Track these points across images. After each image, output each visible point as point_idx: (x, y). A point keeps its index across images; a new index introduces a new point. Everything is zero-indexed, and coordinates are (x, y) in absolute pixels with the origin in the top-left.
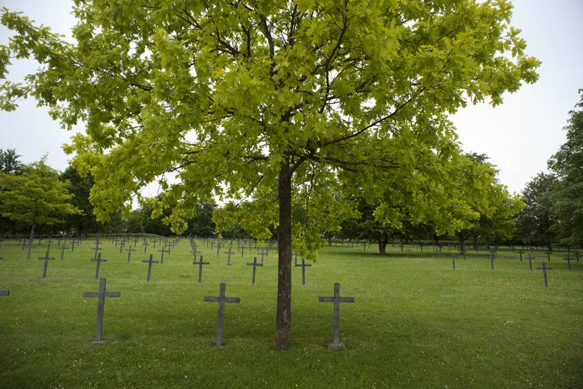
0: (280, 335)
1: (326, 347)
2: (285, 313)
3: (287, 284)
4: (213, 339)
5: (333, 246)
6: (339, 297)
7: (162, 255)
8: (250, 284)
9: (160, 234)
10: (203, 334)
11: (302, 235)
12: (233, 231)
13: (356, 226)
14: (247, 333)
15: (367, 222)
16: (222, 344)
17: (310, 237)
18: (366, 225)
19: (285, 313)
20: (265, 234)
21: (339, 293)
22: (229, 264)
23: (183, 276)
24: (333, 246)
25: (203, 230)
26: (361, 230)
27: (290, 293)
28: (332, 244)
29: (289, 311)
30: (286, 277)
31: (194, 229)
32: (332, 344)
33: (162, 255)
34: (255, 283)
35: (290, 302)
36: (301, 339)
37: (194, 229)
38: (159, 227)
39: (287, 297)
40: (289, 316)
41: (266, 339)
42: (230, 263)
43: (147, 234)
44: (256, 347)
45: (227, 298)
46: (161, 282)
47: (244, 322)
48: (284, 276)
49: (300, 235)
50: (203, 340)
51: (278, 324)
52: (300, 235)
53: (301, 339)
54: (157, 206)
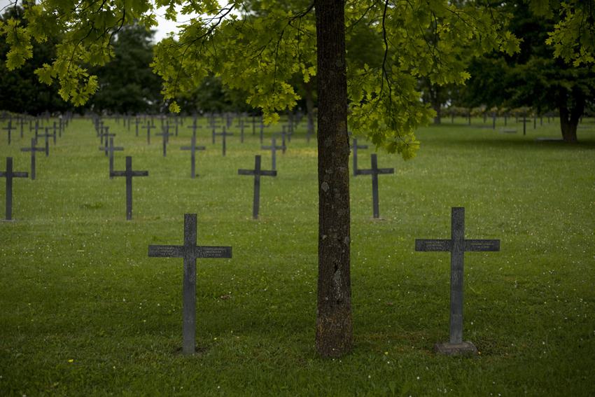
0: (326, 326)
1: (434, 350)
2: (337, 277)
3: (340, 213)
4: (175, 339)
8: (249, 218)
9: (18, 110)
10: (152, 330)
11: (374, 95)
13: (503, 72)
14: (251, 325)
16: (197, 350)
17: (395, 99)
19: (337, 277)
23: (88, 206)
26: (517, 82)
29: (347, 272)
30: (338, 195)
32: (446, 345)
34: (261, 218)
36: (375, 335)
39: (340, 241)
40: (347, 283)
41: (294, 337)
48: (333, 194)
49: (369, 96)
51: (321, 303)
52: (369, 96)
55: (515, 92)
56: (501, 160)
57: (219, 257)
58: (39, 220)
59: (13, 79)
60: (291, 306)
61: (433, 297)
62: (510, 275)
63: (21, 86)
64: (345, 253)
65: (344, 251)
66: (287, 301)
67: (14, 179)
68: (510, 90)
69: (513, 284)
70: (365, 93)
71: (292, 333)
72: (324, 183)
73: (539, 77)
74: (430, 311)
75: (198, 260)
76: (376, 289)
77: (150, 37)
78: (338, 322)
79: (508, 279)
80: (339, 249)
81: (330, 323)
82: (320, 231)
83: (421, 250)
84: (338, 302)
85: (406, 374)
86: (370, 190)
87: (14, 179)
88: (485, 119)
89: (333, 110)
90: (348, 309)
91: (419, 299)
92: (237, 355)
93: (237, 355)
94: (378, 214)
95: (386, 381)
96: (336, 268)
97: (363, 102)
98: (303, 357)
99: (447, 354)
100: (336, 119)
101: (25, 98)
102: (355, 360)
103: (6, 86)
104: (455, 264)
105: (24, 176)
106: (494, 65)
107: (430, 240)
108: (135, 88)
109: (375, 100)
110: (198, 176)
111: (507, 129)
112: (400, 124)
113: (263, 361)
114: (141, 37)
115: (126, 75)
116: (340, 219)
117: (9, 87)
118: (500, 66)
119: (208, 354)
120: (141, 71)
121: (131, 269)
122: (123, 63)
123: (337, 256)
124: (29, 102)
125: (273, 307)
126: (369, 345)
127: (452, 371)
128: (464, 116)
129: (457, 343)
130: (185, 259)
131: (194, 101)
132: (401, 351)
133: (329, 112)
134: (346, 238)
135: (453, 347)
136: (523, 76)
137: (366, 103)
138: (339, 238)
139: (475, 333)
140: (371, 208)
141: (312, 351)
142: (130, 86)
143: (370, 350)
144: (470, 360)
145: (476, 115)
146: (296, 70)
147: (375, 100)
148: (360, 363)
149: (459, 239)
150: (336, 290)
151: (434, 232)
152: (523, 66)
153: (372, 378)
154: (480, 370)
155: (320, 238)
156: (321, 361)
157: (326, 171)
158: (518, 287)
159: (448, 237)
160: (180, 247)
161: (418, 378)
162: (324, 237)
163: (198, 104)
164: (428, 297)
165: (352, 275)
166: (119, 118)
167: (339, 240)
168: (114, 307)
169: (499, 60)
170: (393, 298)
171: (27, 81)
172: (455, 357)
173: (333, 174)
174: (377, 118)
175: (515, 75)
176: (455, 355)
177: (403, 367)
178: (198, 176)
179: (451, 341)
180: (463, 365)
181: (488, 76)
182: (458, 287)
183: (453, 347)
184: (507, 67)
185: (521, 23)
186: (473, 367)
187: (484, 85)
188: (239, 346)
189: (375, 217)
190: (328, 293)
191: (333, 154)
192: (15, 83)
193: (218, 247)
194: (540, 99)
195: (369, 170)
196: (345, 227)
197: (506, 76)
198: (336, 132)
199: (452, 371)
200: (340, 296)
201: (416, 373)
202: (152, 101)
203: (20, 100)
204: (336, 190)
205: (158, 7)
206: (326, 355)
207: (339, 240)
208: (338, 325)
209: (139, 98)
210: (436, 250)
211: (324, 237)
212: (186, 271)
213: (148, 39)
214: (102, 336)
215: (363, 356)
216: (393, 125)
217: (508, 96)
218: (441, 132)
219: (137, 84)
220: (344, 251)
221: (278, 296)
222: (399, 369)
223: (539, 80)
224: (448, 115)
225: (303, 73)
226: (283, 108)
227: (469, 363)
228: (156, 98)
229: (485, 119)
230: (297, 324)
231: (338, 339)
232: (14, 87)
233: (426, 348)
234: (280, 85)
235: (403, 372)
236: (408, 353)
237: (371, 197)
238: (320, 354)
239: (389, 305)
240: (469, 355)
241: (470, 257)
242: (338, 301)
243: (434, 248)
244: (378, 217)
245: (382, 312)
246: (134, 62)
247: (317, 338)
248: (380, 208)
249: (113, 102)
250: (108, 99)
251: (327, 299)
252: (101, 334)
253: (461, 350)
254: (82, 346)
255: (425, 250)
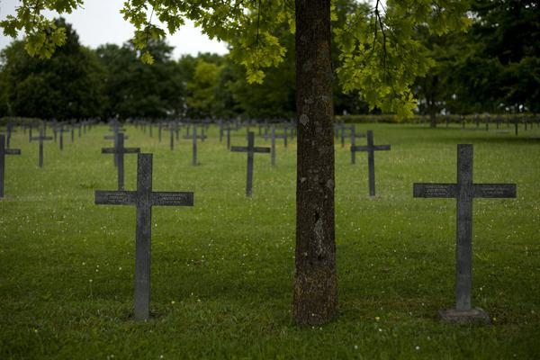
0: (305, 286)
1: (436, 318)
2: (318, 228)
3: (322, 150)
4: (129, 304)
5: (439, 128)
6: (471, 184)
7: (41, 147)
8: (241, 194)
9: (47, 117)
10: (98, 293)
11: (367, 47)
12: (209, 106)
13: (497, 71)
14: (222, 290)
15: (524, 61)
16: (152, 315)
17: (390, 50)
18: (522, 67)
19: (318, 228)
20: (267, 50)
21: (471, 172)
22: (195, 163)
23: (83, 186)
24: (439, 128)
25: (142, 107)
26: (510, 80)
27: (331, 175)
28: (438, 125)
29: (330, 223)
30: (319, 130)
31: (123, 105)
32: (451, 312)
33: (41, 147)
34: (254, 196)
35: (332, 198)
36: (366, 302)
37: (123, 105)
38: (44, 103)
39: (323, 184)
40: (330, 235)
41: (269, 303)
42: (200, 158)
43: (19, 119)
44: (241, 320)
45: (159, 194)
46: (31, 198)
47: (216, 268)
48: (313, 128)
49: (361, 47)
50: (101, 305)
51: (300, 259)
52: (361, 47)
53: (366, 302)
54: (190, 340)
55: (508, 91)
56: (497, 152)
57: (178, 205)
58: (31, 198)
59: (44, 90)
60: (270, 271)
61: (434, 263)
62: (518, 244)
63: (52, 96)
64: (328, 199)
65: (326, 197)
66: (267, 266)
67: (6, 156)
68: (505, 88)
69: (523, 252)
70: (358, 43)
71: (268, 299)
72: (304, 115)
73: (532, 74)
74: (431, 277)
75: (153, 207)
76: (369, 256)
77: (169, 52)
78: (319, 282)
79: (516, 247)
80: (321, 194)
81: (310, 284)
82: (299, 173)
83: (420, 196)
84: (320, 258)
85: (402, 344)
86: (367, 172)
87: (6, 156)
88: (478, 124)
89: (314, 27)
90: (332, 267)
91: (418, 266)
92: (197, 321)
93: (197, 321)
94: (374, 191)
95: (376, 352)
96: (317, 217)
97: (356, 53)
98: (276, 324)
99: (453, 322)
100: (317, 38)
101: (55, 108)
102: (340, 328)
103: (38, 96)
104: (462, 213)
105: (16, 153)
106: (488, 65)
107: (430, 184)
108: (155, 99)
109: (368, 52)
110: (199, 164)
111: (500, 131)
112: (395, 79)
113: (227, 328)
114: (161, 53)
115: (147, 88)
116: (322, 157)
117: (40, 98)
118: (494, 65)
119: (163, 320)
120: (162, 83)
121: (105, 236)
122: (144, 76)
123: (318, 203)
124: (58, 111)
125: (250, 272)
126: (358, 312)
127: (460, 342)
128: (458, 122)
129: (465, 310)
130: (138, 206)
131: (208, 112)
132: (396, 319)
133: (308, 30)
134: (329, 182)
135: (459, 314)
136: (517, 74)
137: (358, 54)
138: (321, 181)
139: (485, 300)
140: (367, 186)
141: (288, 317)
142: (150, 97)
143: (358, 318)
144: (482, 329)
145: (469, 121)
146: (282, 19)
147: (368, 52)
148: (346, 331)
149: (466, 182)
150: (317, 244)
151: (432, 207)
152: (516, 64)
153: (360, 349)
154: (495, 340)
155: (299, 181)
156: (298, 328)
157: (306, 101)
158: (529, 255)
159: (454, 180)
160: (132, 193)
161: (418, 348)
162: (303, 179)
163: (212, 113)
164: (427, 264)
165: (339, 241)
166: (145, 125)
167: (321, 184)
168: (72, 271)
169: (494, 59)
170: (388, 264)
171: (57, 93)
172: (462, 326)
173: (314, 104)
174: (370, 73)
175: (509, 74)
176: (463, 323)
177: (399, 337)
178: (199, 164)
179: (458, 307)
180: (473, 334)
181: (481, 77)
182: (465, 240)
183: (459, 314)
184: (501, 66)
185: (514, 24)
186: (486, 337)
187: (478, 85)
188: (202, 312)
189: (371, 195)
190: (307, 248)
191: (313, 80)
192: (46, 94)
193: (177, 193)
194: (533, 96)
195: (365, 146)
196: (328, 168)
197: (500, 74)
198: (318, 53)
199: (460, 342)
200: (321, 250)
201: (415, 344)
202: (170, 111)
203: (50, 109)
204: (317, 123)
205: (172, 31)
206: (304, 322)
207: (321, 184)
208: (320, 286)
209: (159, 108)
210: (439, 196)
211: (303, 179)
212: (139, 222)
213: (167, 55)
214: (47, 300)
215: (348, 324)
216: (388, 79)
217: (503, 94)
218: (435, 133)
219: (157, 95)
220: (326, 197)
221: (258, 262)
222: (393, 338)
223: (533, 77)
224: (443, 121)
225: (289, 23)
226: (269, 65)
227: (481, 332)
228: (176, 109)
229: (478, 124)
230: (275, 289)
231: (319, 303)
232: (45, 98)
233: (426, 316)
234: (264, 37)
235: (399, 342)
236: (405, 321)
237: (367, 179)
238: (297, 321)
239: (384, 271)
240: (480, 323)
241: (480, 205)
242: (319, 257)
243: (436, 194)
244: (374, 195)
245: (374, 277)
246: (153, 75)
247: (295, 302)
248: (376, 188)
249: (135, 111)
250: (130, 109)
251: (306, 254)
252: (46, 297)
253: (470, 317)
254: (19, 310)
255: (425, 197)
